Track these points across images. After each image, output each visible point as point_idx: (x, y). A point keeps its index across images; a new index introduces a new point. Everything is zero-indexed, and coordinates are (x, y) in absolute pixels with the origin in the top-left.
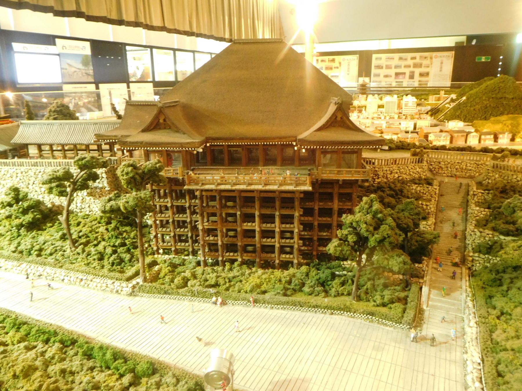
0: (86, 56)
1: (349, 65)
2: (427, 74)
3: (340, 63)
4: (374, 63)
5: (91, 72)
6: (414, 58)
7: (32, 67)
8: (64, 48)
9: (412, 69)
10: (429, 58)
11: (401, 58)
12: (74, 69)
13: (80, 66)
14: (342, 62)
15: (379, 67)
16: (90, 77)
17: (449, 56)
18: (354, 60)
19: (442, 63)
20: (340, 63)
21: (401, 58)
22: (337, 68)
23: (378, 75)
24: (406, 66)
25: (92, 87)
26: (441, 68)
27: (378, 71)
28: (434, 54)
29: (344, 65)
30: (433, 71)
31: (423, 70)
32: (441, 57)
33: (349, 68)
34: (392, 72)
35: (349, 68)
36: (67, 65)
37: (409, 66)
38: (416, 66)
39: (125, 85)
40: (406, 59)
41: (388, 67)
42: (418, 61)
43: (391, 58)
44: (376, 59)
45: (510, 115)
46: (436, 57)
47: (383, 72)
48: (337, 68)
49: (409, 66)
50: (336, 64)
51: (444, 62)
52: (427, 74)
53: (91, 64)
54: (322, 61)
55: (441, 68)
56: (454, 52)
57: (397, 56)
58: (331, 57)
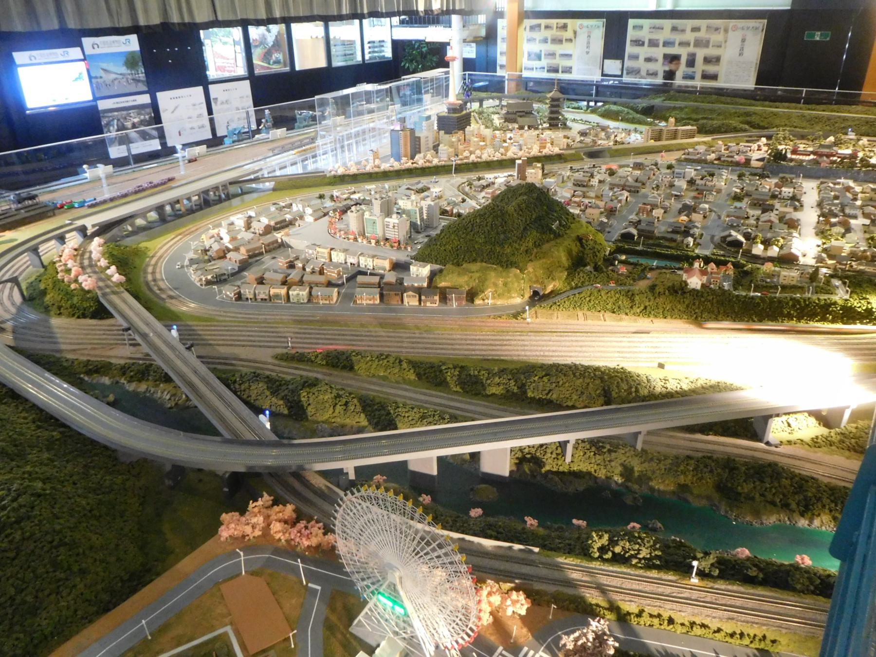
0: (133, 52)
1: (589, 36)
2: (717, 60)
3: (575, 33)
4: (631, 34)
5: (142, 76)
6: (695, 29)
7: (50, 82)
8: (96, 46)
9: (691, 49)
10: (722, 31)
11: (674, 29)
12: (113, 76)
13: (124, 70)
14: (578, 30)
15: (638, 43)
16: (140, 84)
17: (757, 28)
18: (598, 29)
19: (743, 41)
20: (575, 33)
21: (674, 29)
22: (571, 40)
23: (635, 57)
24: (681, 44)
25: (146, 99)
26: (742, 49)
27: (636, 50)
28: (732, 23)
29: (582, 38)
30: (728, 53)
31: (711, 52)
32: (743, 29)
33: (588, 43)
34: (659, 53)
35: (588, 43)
36: (102, 71)
37: (687, 44)
38: (698, 43)
39: (200, 90)
40: (683, 31)
41: (653, 44)
42: (702, 34)
43: (658, 28)
44: (634, 27)
45: (484, 264)
46: (735, 29)
47: (644, 52)
48: (571, 40)
49: (687, 44)
50: (569, 34)
51: (747, 38)
52: (717, 60)
53: (140, 64)
54: (547, 27)
55: (742, 49)
56: (766, 21)
57: (667, 23)
58: (562, 21)
